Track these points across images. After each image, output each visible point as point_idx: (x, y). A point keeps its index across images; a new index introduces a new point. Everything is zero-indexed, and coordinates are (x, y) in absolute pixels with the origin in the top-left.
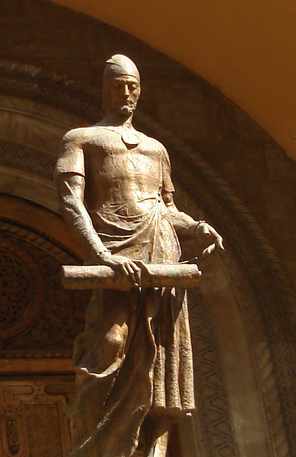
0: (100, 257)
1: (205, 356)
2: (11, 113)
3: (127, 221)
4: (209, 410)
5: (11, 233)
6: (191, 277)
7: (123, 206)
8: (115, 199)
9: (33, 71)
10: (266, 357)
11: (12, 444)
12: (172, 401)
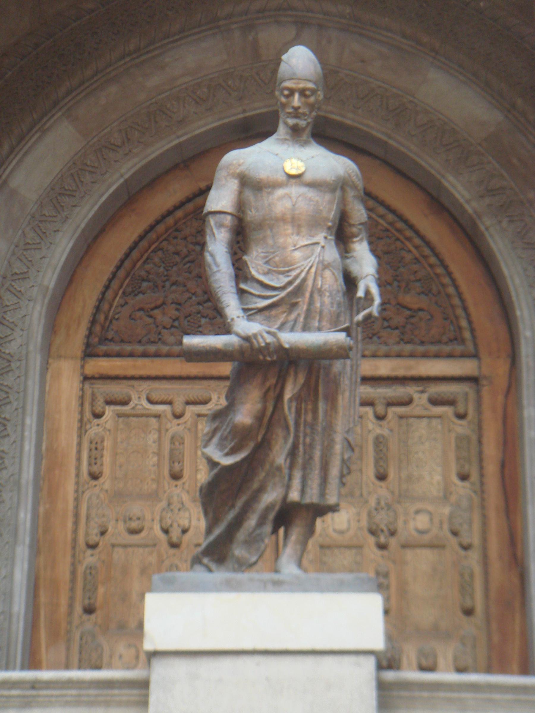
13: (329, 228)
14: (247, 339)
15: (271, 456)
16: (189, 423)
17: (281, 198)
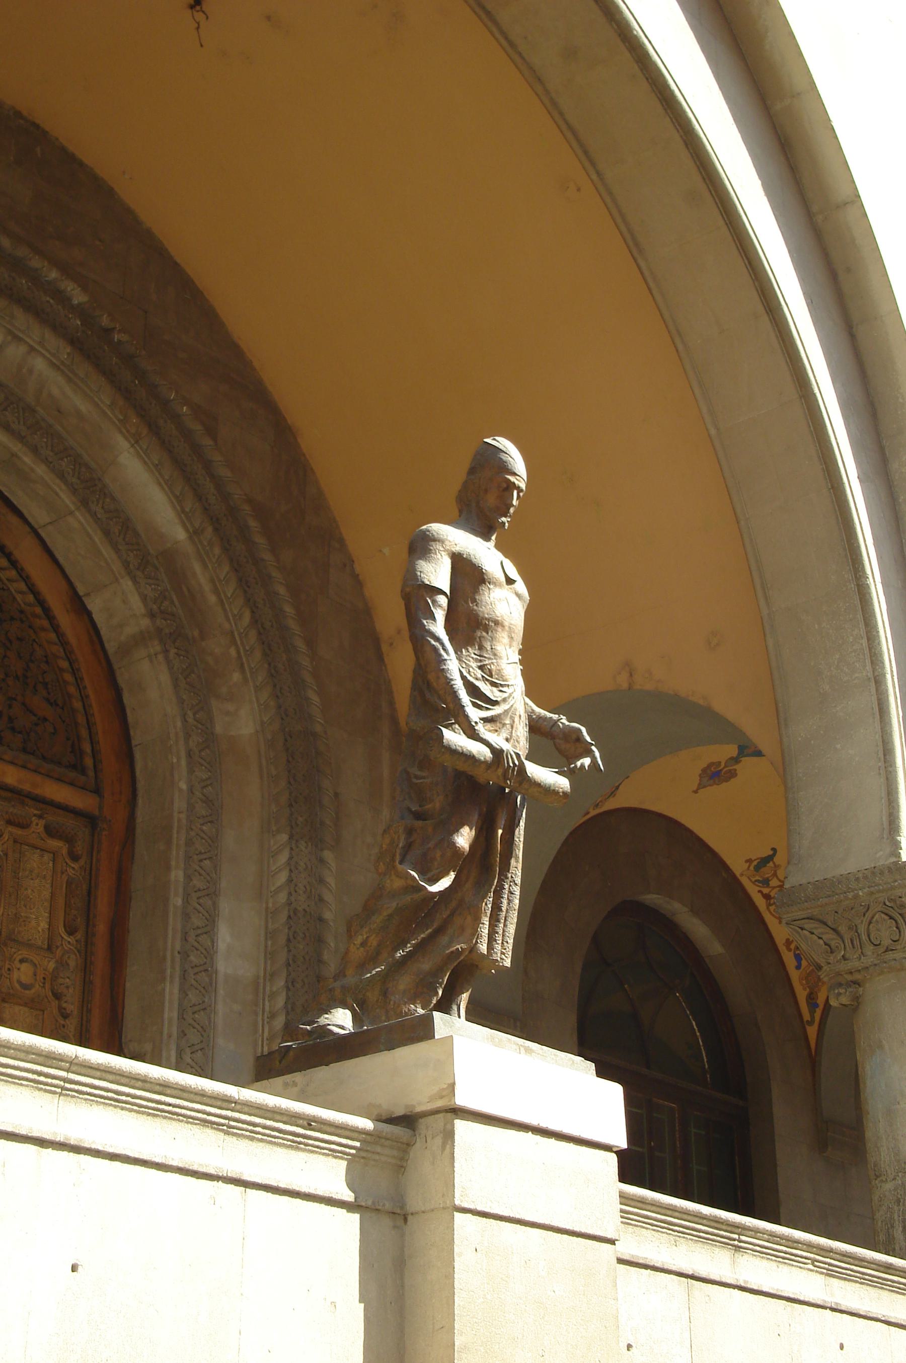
0: (475, 729)
1: (204, 828)
2: (32, 349)
3: (490, 684)
6: (561, 794)
7: (490, 661)
8: (481, 648)
9: (79, 297)
10: (283, 858)
12: (495, 950)
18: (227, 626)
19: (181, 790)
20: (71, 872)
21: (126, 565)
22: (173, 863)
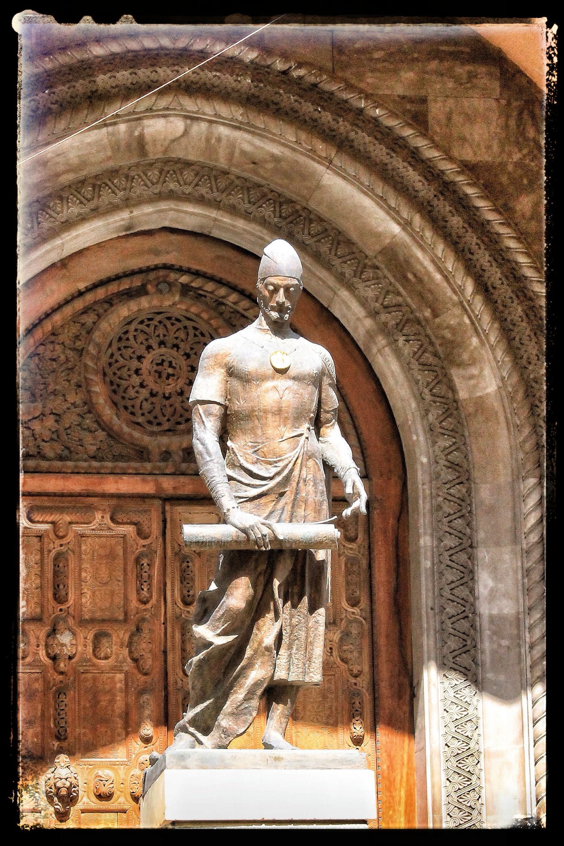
1: (452, 491)
2: (211, 122)
4: (447, 566)
5: (207, 291)
11: (185, 592)
13: (310, 419)
14: (244, 531)
15: (259, 636)
16: (72, 543)
17: (267, 391)
18: (455, 298)
19: (422, 463)
20: (349, 553)
21: (341, 278)
22: (421, 531)
